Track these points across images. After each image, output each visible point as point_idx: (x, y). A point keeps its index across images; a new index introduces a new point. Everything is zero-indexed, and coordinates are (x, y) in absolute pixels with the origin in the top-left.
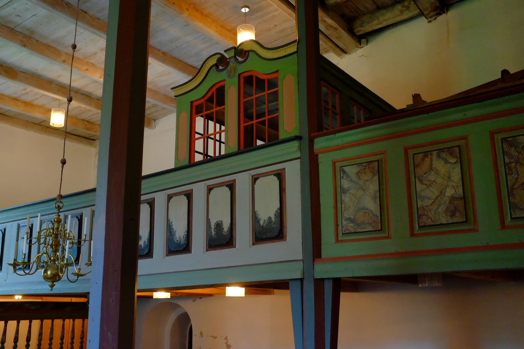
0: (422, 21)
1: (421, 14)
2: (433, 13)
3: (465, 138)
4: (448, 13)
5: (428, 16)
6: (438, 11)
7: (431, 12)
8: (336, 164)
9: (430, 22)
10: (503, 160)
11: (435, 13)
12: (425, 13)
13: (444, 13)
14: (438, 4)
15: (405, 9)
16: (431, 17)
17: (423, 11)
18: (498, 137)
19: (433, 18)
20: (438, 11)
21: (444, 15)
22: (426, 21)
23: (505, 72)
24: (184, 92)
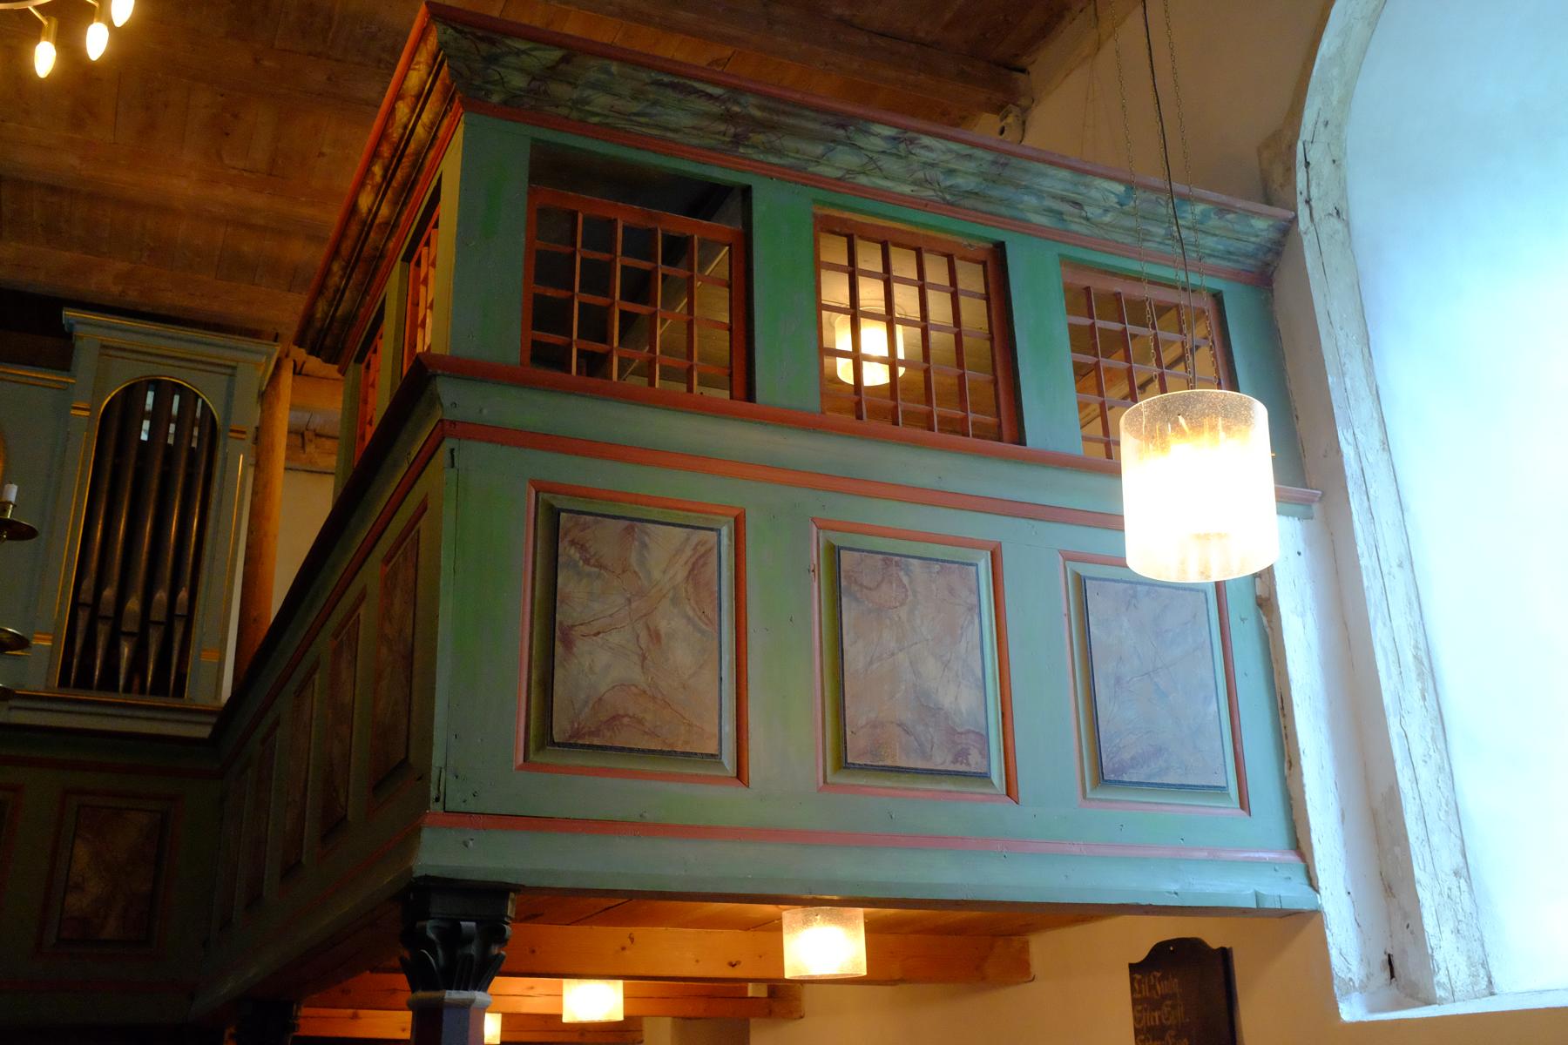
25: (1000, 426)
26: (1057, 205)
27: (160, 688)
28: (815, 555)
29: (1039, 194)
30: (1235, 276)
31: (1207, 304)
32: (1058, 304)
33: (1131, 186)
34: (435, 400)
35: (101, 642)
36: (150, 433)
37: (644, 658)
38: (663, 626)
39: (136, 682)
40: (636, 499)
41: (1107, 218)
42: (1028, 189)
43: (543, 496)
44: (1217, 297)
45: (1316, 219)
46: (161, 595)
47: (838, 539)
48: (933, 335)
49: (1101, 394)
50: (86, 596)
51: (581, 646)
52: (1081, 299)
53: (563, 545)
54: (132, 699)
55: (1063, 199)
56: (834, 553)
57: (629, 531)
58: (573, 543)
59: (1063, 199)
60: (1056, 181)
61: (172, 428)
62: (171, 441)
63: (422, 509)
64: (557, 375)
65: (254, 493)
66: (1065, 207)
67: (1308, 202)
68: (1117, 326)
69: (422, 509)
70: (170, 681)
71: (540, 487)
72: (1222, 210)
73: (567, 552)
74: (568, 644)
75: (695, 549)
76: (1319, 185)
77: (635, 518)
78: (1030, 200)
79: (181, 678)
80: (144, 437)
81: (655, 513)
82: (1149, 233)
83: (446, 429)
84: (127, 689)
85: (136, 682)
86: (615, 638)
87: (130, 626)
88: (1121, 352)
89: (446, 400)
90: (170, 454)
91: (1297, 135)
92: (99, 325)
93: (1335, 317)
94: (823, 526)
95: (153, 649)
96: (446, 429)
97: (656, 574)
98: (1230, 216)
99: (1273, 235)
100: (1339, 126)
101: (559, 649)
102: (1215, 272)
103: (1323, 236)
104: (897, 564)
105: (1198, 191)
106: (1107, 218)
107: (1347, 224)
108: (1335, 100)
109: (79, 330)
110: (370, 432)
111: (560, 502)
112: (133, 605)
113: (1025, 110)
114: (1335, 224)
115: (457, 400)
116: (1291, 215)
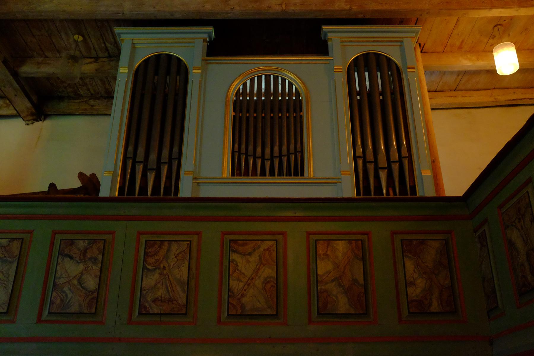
0: (19, 123)
1: (18, 115)
2: (29, 118)
3: (31, 232)
4: (45, 122)
5: (25, 119)
6: (35, 117)
7: (27, 115)
8: (196, 236)
9: (28, 124)
10: (228, 256)
11: (32, 118)
12: (22, 115)
13: (41, 120)
14: (34, 111)
15: (5, 105)
16: (29, 120)
17: (20, 113)
18: (143, 239)
19: (30, 122)
20: (35, 117)
21: (40, 122)
22: (24, 123)
23: (52, 186)
24: (120, 114)
87: (383, 162)
109: (330, 35)
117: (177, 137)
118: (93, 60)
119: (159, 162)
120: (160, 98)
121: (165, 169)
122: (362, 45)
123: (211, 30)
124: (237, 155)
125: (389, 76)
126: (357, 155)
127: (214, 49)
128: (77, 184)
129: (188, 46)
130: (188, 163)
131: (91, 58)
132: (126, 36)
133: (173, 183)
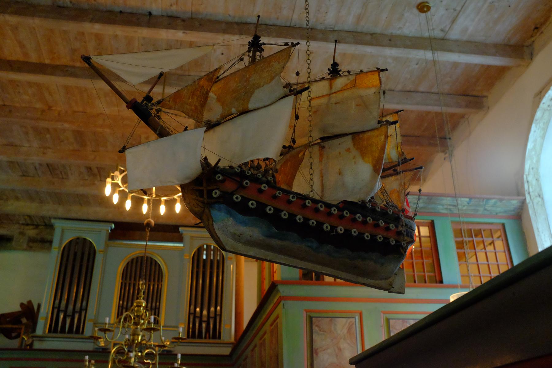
25: (435, 276)
26: (449, 207)
27: (214, 337)
28: (383, 322)
29: (443, 205)
30: (509, 217)
31: (500, 227)
32: (451, 235)
33: (471, 198)
34: (278, 291)
35: (197, 325)
36: (207, 255)
37: (337, 356)
38: (342, 346)
39: (208, 335)
40: (333, 312)
41: (465, 208)
42: (440, 204)
43: (308, 313)
44: (503, 225)
45: (532, 198)
46: (212, 309)
47: (389, 316)
48: (423, 239)
49: (475, 249)
50: (192, 311)
51: (320, 354)
52: (458, 233)
53: (314, 326)
54: (207, 341)
55: (450, 205)
56: (388, 320)
57: (331, 321)
58: (317, 326)
59: (450, 205)
60: (447, 201)
61: (212, 252)
62: (212, 258)
63: (277, 317)
64: (310, 281)
65: (236, 274)
66: (451, 207)
67: (529, 193)
68: (471, 239)
69: (277, 317)
70: (216, 335)
71: (307, 311)
72: (501, 200)
73: (315, 328)
74: (317, 354)
75: (349, 324)
76: (532, 188)
77: (332, 317)
78: (441, 207)
79: (220, 333)
80: (204, 257)
81: (338, 315)
82: (478, 210)
83: (281, 299)
84: (205, 338)
85: (208, 335)
86: (329, 351)
87: (205, 319)
88: (480, 236)
89: (281, 290)
90: (212, 262)
91: (523, 173)
92: (191, 231)
93: (540, 230)
94: (384, 313)
95: (211, 326)
96: (281, 299)
97: (339, 332)
98: (504, 201)
99: (519, 204)
100: (537, 169)
101: (314, 355)
102: (502, 217)
103: (535, 204)
104: (406, 322)
105: (492, 196)
106: (465, 208)
107: (543, 199)
108: (534, 161)
109: (184, 233)
110: (265, 293)
111: (313, 315)
112: (205, 312)
113: (452, 151)
114: (539, 199)
115: (283, 290)
116: (524, 198)
117: (88, 278)
118: (34, 227)
119: (74, 311)
120: (78, 263)
121: (77, 316)
122: (167, 330)
123: (113, 226)
124: (120, 308)
125: (218, 260)
126: (288, 93)
127: (114, 236)
128: (17, 308)
129: (97, 236)
130: (91, 312)
131: (33, 225)
132: (58, 225)
133: (81, 326)
